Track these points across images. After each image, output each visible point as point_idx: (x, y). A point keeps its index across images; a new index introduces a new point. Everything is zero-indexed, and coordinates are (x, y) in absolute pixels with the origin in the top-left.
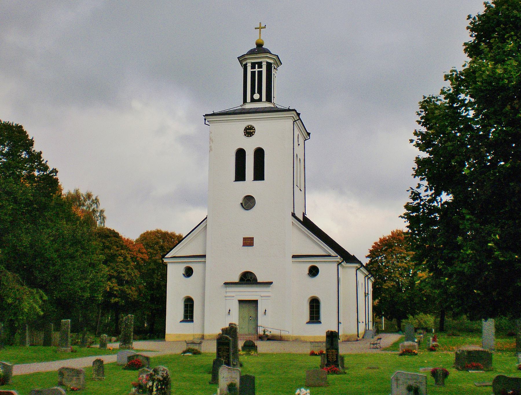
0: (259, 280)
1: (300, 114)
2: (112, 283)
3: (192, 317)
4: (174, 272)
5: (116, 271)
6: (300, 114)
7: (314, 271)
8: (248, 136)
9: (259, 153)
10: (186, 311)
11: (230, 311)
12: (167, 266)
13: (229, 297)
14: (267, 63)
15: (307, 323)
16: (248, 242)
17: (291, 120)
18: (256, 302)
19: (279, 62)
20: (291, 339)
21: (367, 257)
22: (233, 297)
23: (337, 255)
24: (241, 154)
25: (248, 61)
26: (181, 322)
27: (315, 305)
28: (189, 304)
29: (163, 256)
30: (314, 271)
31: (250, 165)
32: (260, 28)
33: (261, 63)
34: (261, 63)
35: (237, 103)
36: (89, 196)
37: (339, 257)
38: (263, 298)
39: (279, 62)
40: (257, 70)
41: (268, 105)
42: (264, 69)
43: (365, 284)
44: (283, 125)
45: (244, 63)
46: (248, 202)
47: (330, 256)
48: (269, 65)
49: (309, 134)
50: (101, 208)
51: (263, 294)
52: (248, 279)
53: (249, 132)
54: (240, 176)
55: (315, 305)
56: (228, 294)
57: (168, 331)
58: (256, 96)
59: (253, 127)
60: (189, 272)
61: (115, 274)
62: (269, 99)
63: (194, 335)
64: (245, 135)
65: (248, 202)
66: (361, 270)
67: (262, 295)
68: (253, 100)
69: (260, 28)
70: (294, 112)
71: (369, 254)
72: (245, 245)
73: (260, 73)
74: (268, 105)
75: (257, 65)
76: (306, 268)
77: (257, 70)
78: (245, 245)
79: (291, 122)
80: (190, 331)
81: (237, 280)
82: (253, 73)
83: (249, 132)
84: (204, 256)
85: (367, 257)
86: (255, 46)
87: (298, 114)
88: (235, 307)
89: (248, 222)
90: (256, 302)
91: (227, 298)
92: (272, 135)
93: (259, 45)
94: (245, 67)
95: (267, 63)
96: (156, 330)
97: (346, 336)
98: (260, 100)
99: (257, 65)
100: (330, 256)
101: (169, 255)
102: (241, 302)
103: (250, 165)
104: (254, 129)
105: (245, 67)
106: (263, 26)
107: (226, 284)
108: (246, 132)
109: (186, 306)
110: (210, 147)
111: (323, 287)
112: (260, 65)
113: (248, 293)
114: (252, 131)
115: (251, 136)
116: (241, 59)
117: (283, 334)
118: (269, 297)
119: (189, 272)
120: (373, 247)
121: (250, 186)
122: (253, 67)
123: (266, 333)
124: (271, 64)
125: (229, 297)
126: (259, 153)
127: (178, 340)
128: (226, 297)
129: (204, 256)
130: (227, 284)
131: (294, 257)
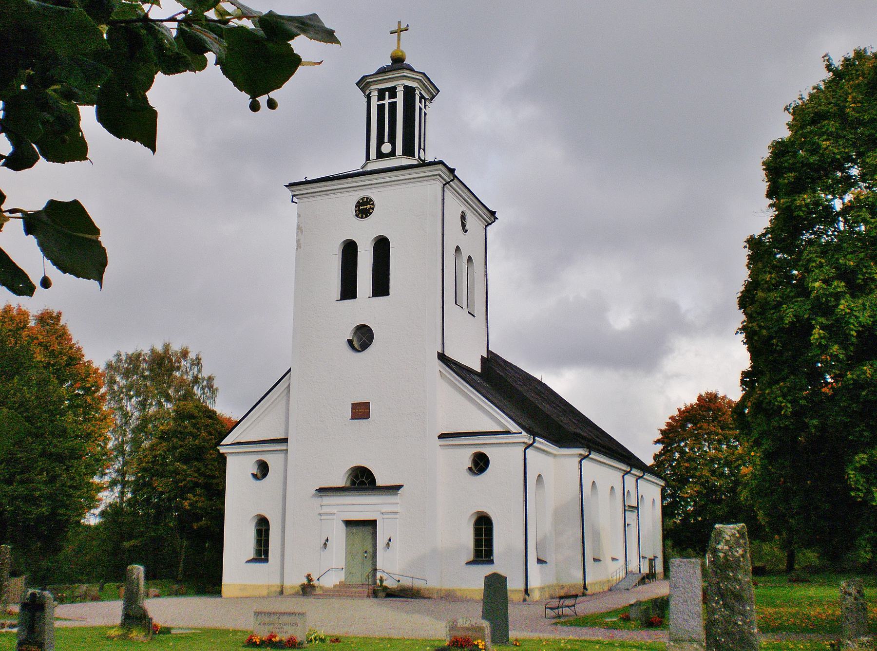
0: (379, 482)
1: (454, 170)
2: (195, 496)
3: (266, 553)
4: (238, 470)
5: (203, 474)
6: (454, 170)
7: (480, 463)
8: (362, 218)
9: (382, 246)
10: (478, 542)
11: (390, 540)
12: (225, 458)
13: (327, 514)
14: (406, 87)
15: (469, 563)
16: (361, 411)
17: (437, 182)
18: (373, 523)
19: (433, 92)
20: (435, 596)
21: (658, 442)
22: (334, 514)
23: (513, 427)
24: (350, 250)
25: (372, 87)
26: (248, 562)
27: (483, 526)
28: (263, 526)
29: (218, 444)
30: (480, 463)
31: (365, 269)
32: (399, 31)
33: (395, 88)
34: (395, 88)
35: (356, 163)
36: (185, 354)
37: (524, 433)
38: (385, 516)
39: (433, 92)
40: (387, 101)
41: (407, 161)
42: (400, 100)
43: (651, 492)
44: (427, 190)
45: (367, 92)
46: (363, 337)
47: (508, 432)
48: (409, 92)
49: (493, 213)
50: (205, 373)
51: (385, 509)
52: (362, 480)
53: (364, 209)
54: (349, 290)
55: (483, 526)
56: (326, 510)
57: (226, 579)
58: (386, 148)
59: (371, 200)
60: (263, 469)
61: (201, 480)
62: (408, 151)
63: (268, 587)
64: (357, 216)
65: (363, 337)
66: (592, 459)
67: (384, 510)
68: (380, 155)
69: (399, 31)
70: (441, 167)
71: (660, 437)
72: (355, 416)
73: (393, 106)
74: (407, 161)
75: (387, 93)
76: (465, 457)
77: (387, 101)
78: (355, 416)
79: (438, 185)
80: (264, 576)
81: (341, 481)
82: (381, 108)
83: (364, 209)
84: (285, 441)
85: (658, 442)
86: (389, 62)
87: (452, 171)
88: (338, 534)
89: (361, 375)
90: (373, 523)
91: (323, 517)
92: (405, 210)
93: (398, 62)
94: (369, 98)
95: (406, 87)
96: (206, 578)
97: (562, 587)
98: (393, 154)
99: (387, 93)
100: (508, 432)
101: (227, 441)
102: (348, 523)
103: (365, 269)
104: (373, 204)
105: (369, 98)
106: (403, 26)
107: (322, 490)
108: (359, 209)
109: (478, 532)
110: (298, 241)
111: (495, 494)
112: (393, 92)
113: (361, 506)
114: (369, 206)
115: (367, 216)
116: (363, 84)
117: (418, 584)
118: (396, 513)
119: (263, 469)
120: (668, 424)
121: (365, 307)
122: (381, 97)
123: (385, 584)
124: (413, 89)
125: (327, 514)
126: (382, 246)
127: (245, 594)
128: (320, 515)
129: (285, 441)
130: (323, 491)
131: (442, 436)
